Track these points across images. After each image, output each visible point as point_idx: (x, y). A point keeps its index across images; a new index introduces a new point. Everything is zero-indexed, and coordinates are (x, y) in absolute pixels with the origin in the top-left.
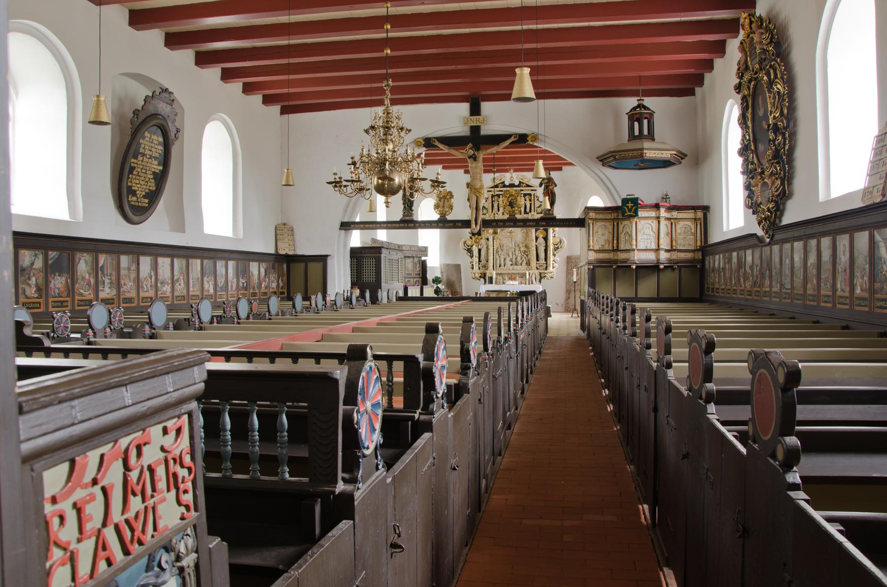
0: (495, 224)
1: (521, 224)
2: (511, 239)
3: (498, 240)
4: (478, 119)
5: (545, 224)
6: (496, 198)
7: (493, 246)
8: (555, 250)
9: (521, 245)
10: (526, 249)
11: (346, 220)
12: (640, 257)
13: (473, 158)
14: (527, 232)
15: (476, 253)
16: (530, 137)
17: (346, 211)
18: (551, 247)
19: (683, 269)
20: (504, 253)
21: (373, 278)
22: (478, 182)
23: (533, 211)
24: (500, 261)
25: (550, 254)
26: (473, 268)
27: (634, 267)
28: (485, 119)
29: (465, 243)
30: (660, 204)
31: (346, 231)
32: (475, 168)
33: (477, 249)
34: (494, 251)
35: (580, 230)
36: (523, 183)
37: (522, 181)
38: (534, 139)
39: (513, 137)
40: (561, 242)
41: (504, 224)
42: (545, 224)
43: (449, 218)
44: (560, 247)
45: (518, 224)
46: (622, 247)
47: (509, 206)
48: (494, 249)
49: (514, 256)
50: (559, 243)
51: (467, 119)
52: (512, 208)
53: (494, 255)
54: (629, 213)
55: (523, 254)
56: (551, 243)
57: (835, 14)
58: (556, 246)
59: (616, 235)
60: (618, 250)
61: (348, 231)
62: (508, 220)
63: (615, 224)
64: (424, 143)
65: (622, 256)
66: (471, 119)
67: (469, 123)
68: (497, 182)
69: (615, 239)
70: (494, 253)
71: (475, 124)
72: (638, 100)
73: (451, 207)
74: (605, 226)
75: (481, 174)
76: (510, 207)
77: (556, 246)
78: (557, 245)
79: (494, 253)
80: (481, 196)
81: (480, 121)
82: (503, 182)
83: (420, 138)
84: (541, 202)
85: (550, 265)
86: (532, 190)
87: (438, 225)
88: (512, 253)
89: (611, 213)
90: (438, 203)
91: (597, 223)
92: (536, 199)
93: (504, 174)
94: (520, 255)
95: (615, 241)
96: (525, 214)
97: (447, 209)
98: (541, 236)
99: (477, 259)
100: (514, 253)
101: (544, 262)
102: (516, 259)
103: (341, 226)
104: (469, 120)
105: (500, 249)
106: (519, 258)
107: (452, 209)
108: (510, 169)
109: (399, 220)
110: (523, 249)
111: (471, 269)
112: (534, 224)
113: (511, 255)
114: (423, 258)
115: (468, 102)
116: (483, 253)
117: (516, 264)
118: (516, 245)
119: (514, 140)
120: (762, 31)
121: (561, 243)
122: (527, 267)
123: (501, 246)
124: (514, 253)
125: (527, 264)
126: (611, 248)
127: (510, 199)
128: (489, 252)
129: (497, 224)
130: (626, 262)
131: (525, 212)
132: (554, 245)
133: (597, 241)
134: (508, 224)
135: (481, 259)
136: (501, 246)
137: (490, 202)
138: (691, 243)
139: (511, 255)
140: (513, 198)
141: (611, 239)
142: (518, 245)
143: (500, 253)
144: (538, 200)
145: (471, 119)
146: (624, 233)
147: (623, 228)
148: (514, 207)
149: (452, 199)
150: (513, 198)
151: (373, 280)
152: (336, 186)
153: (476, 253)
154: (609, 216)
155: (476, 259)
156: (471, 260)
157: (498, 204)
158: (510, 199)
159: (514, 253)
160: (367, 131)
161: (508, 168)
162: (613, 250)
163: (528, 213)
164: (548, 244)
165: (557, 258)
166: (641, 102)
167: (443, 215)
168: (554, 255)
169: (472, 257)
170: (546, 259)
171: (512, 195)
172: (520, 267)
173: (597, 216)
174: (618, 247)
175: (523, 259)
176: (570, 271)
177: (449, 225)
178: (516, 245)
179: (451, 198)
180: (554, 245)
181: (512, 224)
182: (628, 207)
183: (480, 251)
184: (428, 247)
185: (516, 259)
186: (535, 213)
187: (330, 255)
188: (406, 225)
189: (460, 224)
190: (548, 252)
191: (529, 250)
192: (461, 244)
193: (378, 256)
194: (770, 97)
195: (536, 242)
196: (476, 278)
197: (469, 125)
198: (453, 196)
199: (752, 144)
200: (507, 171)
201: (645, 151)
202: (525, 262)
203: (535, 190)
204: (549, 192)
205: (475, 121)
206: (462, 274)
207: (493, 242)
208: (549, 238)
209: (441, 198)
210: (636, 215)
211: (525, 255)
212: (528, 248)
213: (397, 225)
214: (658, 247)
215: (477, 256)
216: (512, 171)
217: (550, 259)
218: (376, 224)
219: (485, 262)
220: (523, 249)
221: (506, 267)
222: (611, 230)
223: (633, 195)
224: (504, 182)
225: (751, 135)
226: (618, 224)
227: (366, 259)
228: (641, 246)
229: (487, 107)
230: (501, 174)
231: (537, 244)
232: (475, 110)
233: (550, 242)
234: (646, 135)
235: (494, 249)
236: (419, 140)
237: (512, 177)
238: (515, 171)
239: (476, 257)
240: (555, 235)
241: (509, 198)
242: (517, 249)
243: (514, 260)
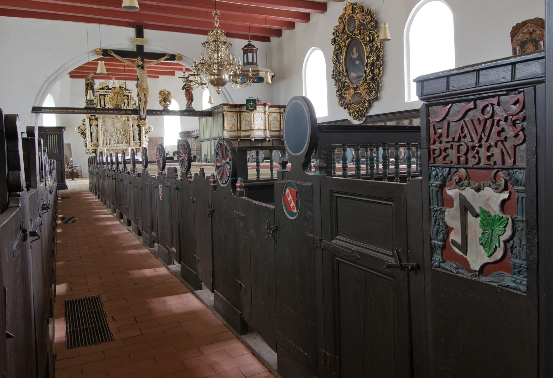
0: (155, 113)
6: (102, 97)
9: (121, 130)
11: (36, 105)
12: (258, 134)
13: (141, 67)
16: (177, 57)
17: (36, 99)
19: (274, 141)
20: (108, 135)
21: (56, 150)
24: (106, 141)
25: (143, 136)
26: (86, 146)
27: (253, 140)
28: (147, 41)
30: (267, 104)
31: (36, 114)
35: (199, 119)
36: (123, 88)
37: (122, 86)
38: (179, 58)
39: (167, 56)
46: (243, 128)
49: (116, 137)
52: (165, 103)
54: (251, 108)
55: (123, 136)
57: (416, 14)
58: (146, 131)
59: (239, 121)
60: (240, 130)
61: (38, 114)
63: (238, 114)
64: (102, 53)
65: (243, 134)
66: (137, 40)
67: (136, 42)
68: (104, 85)
69: (239, 123)
72: (248, 41)
74: (232, 115)
75: (146, 79)
78: (146, 130)
81: (144, 41)
82: (108, 86)
84: (135, 101)
85: (143, 143)
86: (129, 93)
87: (114, 112)
89: (235, 108)
92: (131, 99)
93: (108, 80)
95: (239, 125)
99: (90, 140)
101: (138, 141)
102: (118, 139)
105: (105, 133)
106: (120, 139)
108: (112, 77)
109: (84, 107)
110: (123, 133)
111: (85, 147)
113: (114, 137)
115: (134, 27)
116: (94, 135)
117: (118, 143)
119: (167, 58)
120: (364, 14)
121: (149, 128)
122: (126, 145)
125: (126, 142)
126: (236, 129)
127: (164, 96)
129: (156, 113)
130: (249, 137)
135: (93, 139)
137: (99, 99)
138: (277, 127)
139: (114, 137)
140: (166, 96)
141: (235, 123)
142: (119, 130)
143: (106, 135)
144: (133, 99)
145: (137, 40)
146: (244, 120)
147: (244, 117)
151: (56, 152)
154: (234, 110)
155: (88, 139)
156: (85, 140)
157: (105, 101)
160: (203, 44)
161: (111, 76)
162: (237, 130)
166: (250, 42)
168: (145, 137)
170: (140, 139)
171: (166, 94)
172: (122, 144)
174: (240, 128)
176: (151, 148)
177: (122, 112)
182: (250, 105)
185: (118, 139)
188: (89, 111)
189: (130, 112)
192: (76, 129)
193: (60, 134)
194: (366, 49)
196: (89, 153)
197: (136, 43)
199: (345, 72)
200: (110, 78)
201: (260, 72)
202: (125, 141)
203: (131, 93)
205: (139, 41)
206: (72, 150)
210: (255, 108)
213: (82, 111)
214: (265, 128)
215: (90, 137)
216: (114, 78)
219: (96, 141)
220: (123, 133)
221: (111, 145)
222: (236, 118)
223: (253, 98)
225: (344, 67)
226: (240, 115)
227: (49, 136)
228: (256, 128)
229: (147, 32)
230: (106, 80)
232: (140, 34)
234: (255, 63)
236: (98, 50)
237: (114, 83)
238: (117, 79)
239: (89, 138)
242: (118, 132)
243: (117, 140)
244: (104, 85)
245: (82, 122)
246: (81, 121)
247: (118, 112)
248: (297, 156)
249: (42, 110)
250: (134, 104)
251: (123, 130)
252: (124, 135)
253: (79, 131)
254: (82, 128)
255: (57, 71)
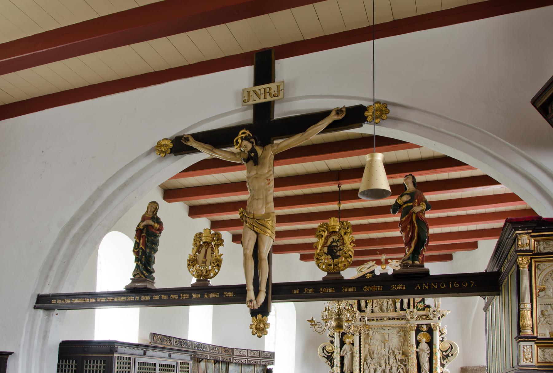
1: (352, 290)
2: (384, 344)
3: (367, 345)
4: (268, 90)
5: (404, 288)
7: (360, 353)
8: (444, 359)
9: (397, 352)
10: (403, 357)
11: (47, 291)
14: (405, 335)
15: (337, 361)
16: (371, 111)
18: (438, 355)
22: (260, 206)
23: (412, 307)
25: (436, 364)
28: (281, 88)
29: (324, 348)
32: (256, 178)
33: (339, 357)
34: (360, 359)
39: (333, 113)
40: (451, 347)
41: (317, 291)
42: (404, 288)
43: (213, 282)
44: (451, 355)
45: (345, 290)
47: (327, 254)
48: (360, 356)
49: (388, 366)
50: (450, 350)
51: (248, 92)
52: (333, 259)
53: (360, 365)
55: (399, 363)
56: (438, 348)
58: (444, 353)
62: (325, 283)
66: (255, 92)
67: (251, 98)
70: (360, 362)
71: (262, 100)
73: (218, 263)
76: (329, 257)
77: (444, 353)
78: (446, 352)
79: (360, 362)
80: (266, 232)
81: (272, 91)
83: (167, 139)
88: (385, 362)
90: (195, 256)
91: (542, 266)
94: (395, 364)
96: (401, 311)
97: (210, 267)
98: (424, 340)
100: (388, 362)
103: (37, 303)
104: (252, 93)
107: (219, 266)
109: (122, 288)
110: (399, 357)
112: (380, 289)
114: (269, 367)
116: (346, 362)
118: (391, 351)
123: (371, 353)
124: (387, 362)
127: (331, 240)
128: (354, 360)
129: (302, 291)
131: (402, 309)
132: (442, 352)
133: (542, 312)
134: (325, 290)
135: (344, 368)
136: (371, 353)
140: (336, 238)
142: (394, 352)
143: (369, 361)
148: (338, 257)
149: (220, 248)
150: (336, 238)
152: (312, 325)
153: (337, 361)
158: (331, 240)
159: (387, 362)
163: (405, 310)
164: (434, 350)
165: (446, 369)
167: (203, 277)
168: (443, 365)
169: (332, 366)
173: (542, 248)
175: (400, 370)
178: (391, 351)
179: (218, 245)
180: (442, 352)
181: (333, 290)
183: (342, 358)
184: (274, 353)
186: (415, 310)
187: (11, 353)
189: (231, 295)
190: (434, 362)
191: (408, 359)
192: (320, 350)
195: (417, 348)
197: (251, 102)
198: (223, 241)
204: (412, 219)
207: (360, 347)
208: (434, 343)
209: (201, 245)
211: (401, 365)
212: (407, 356)
215: (339, 365)
217: (436, 370)
218: (90, 298)
220: (399, 357)
224: (373, 271)
231: (418, 350)
233: (436, 348)
235: (360, 356)
240: (443, 338)
241: (327, 237)
242: (392, 357)
244: (365, 270)
245: (330, 339)
246: (328, 336)
247: (202, 296)
248: (234, 139)
249: (54, 301)
250: (420, 302)
251: (401, 352)
252: (402, 361)
253: (323, 354)
254: (329, 348)
255: (83, 209)
